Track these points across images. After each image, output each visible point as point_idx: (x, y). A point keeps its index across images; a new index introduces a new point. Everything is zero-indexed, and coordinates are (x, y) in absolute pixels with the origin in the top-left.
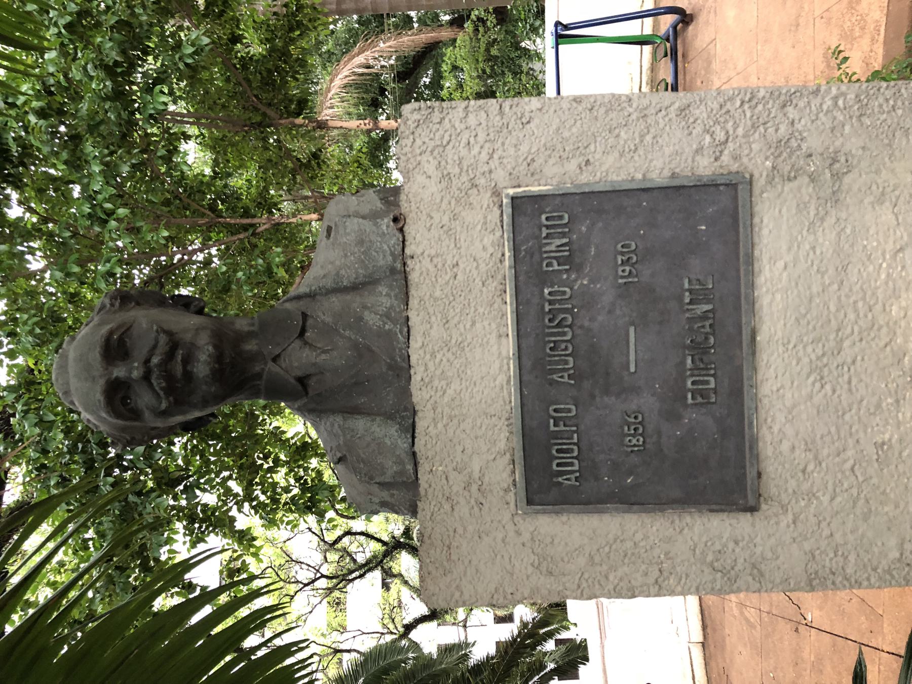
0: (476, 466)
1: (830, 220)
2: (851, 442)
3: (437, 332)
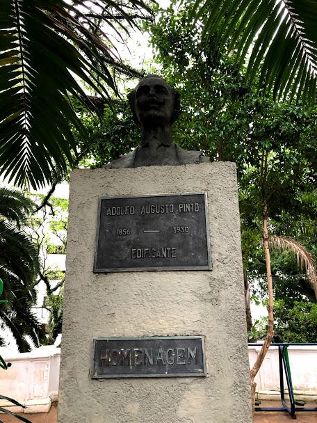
0: (115, 185)
1: (195, 298)
2: (115, 305)
3: (160, 173)
